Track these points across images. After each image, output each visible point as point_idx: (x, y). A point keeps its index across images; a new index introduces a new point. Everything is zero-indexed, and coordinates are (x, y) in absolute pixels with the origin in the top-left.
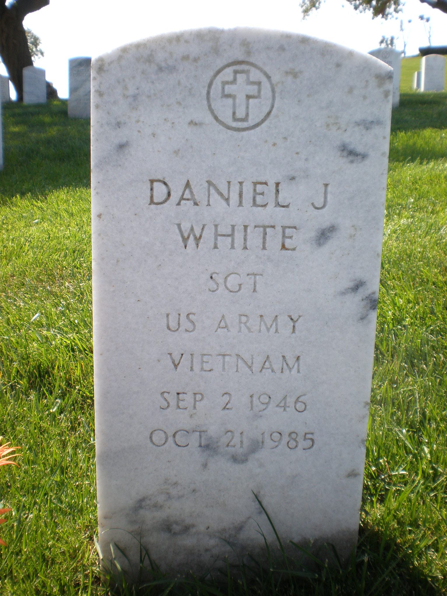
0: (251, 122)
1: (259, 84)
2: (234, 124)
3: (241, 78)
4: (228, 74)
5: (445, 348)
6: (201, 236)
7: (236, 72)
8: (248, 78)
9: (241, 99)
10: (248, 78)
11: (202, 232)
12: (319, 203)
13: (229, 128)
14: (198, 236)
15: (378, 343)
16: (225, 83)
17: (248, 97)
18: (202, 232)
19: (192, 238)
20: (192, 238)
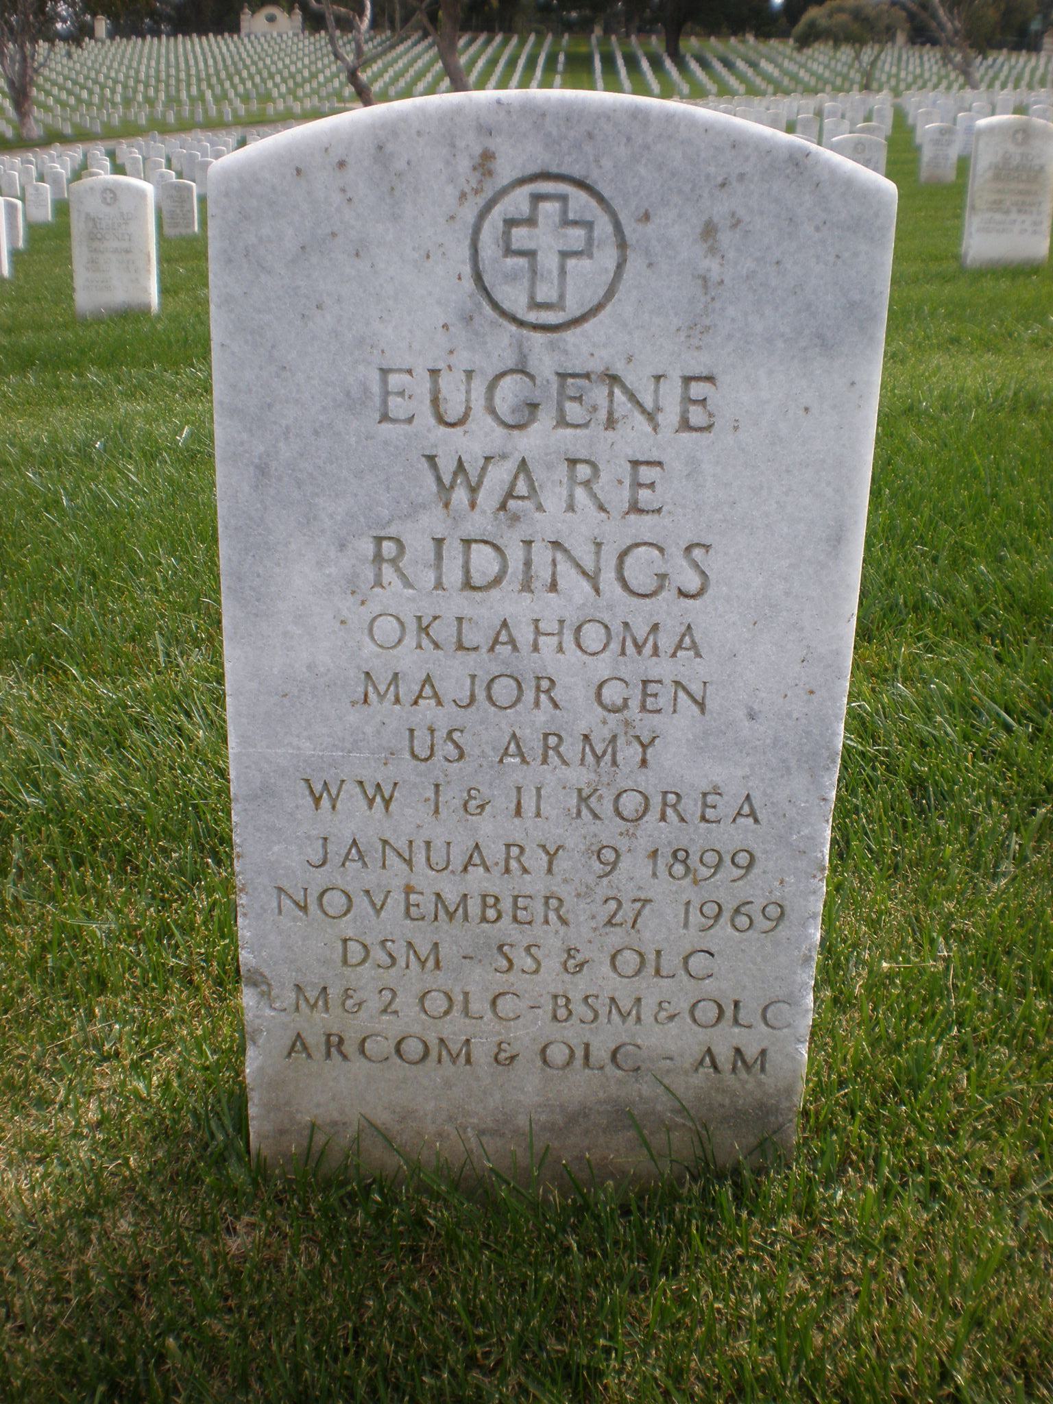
0: (573, 308)
1: (589, 225)
2: (532, 317)
3: (549, 208)
4: (517, 203)
5: (10, 1085)
6: (391, 797)
7: (537, 198)
8: (565, 212)
9: (549, 261)
10: (565, 212)
11: (598, 561)
12: (316, 859)
13: (521, 323)
14: (387, 796)
15: (844, 793)
16: (510, 223)
17: (565, 255)
18: (598, 561)
19: (378, 799)
20: (378, 799)
